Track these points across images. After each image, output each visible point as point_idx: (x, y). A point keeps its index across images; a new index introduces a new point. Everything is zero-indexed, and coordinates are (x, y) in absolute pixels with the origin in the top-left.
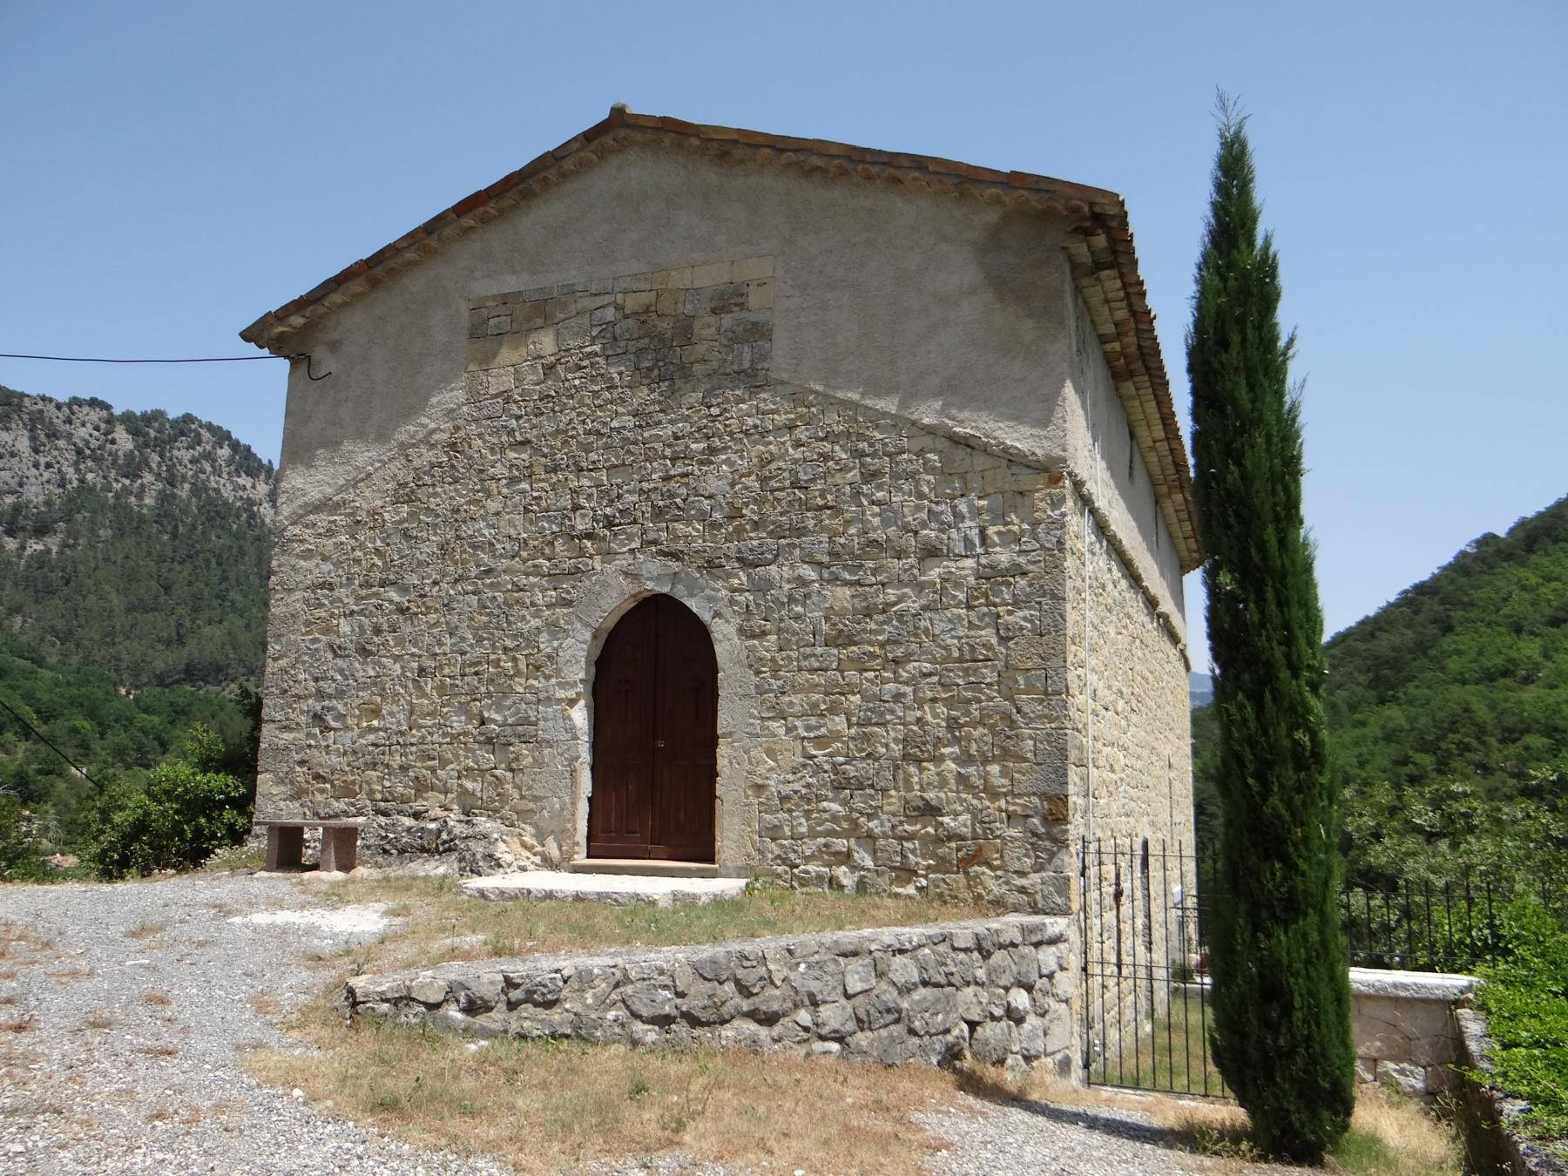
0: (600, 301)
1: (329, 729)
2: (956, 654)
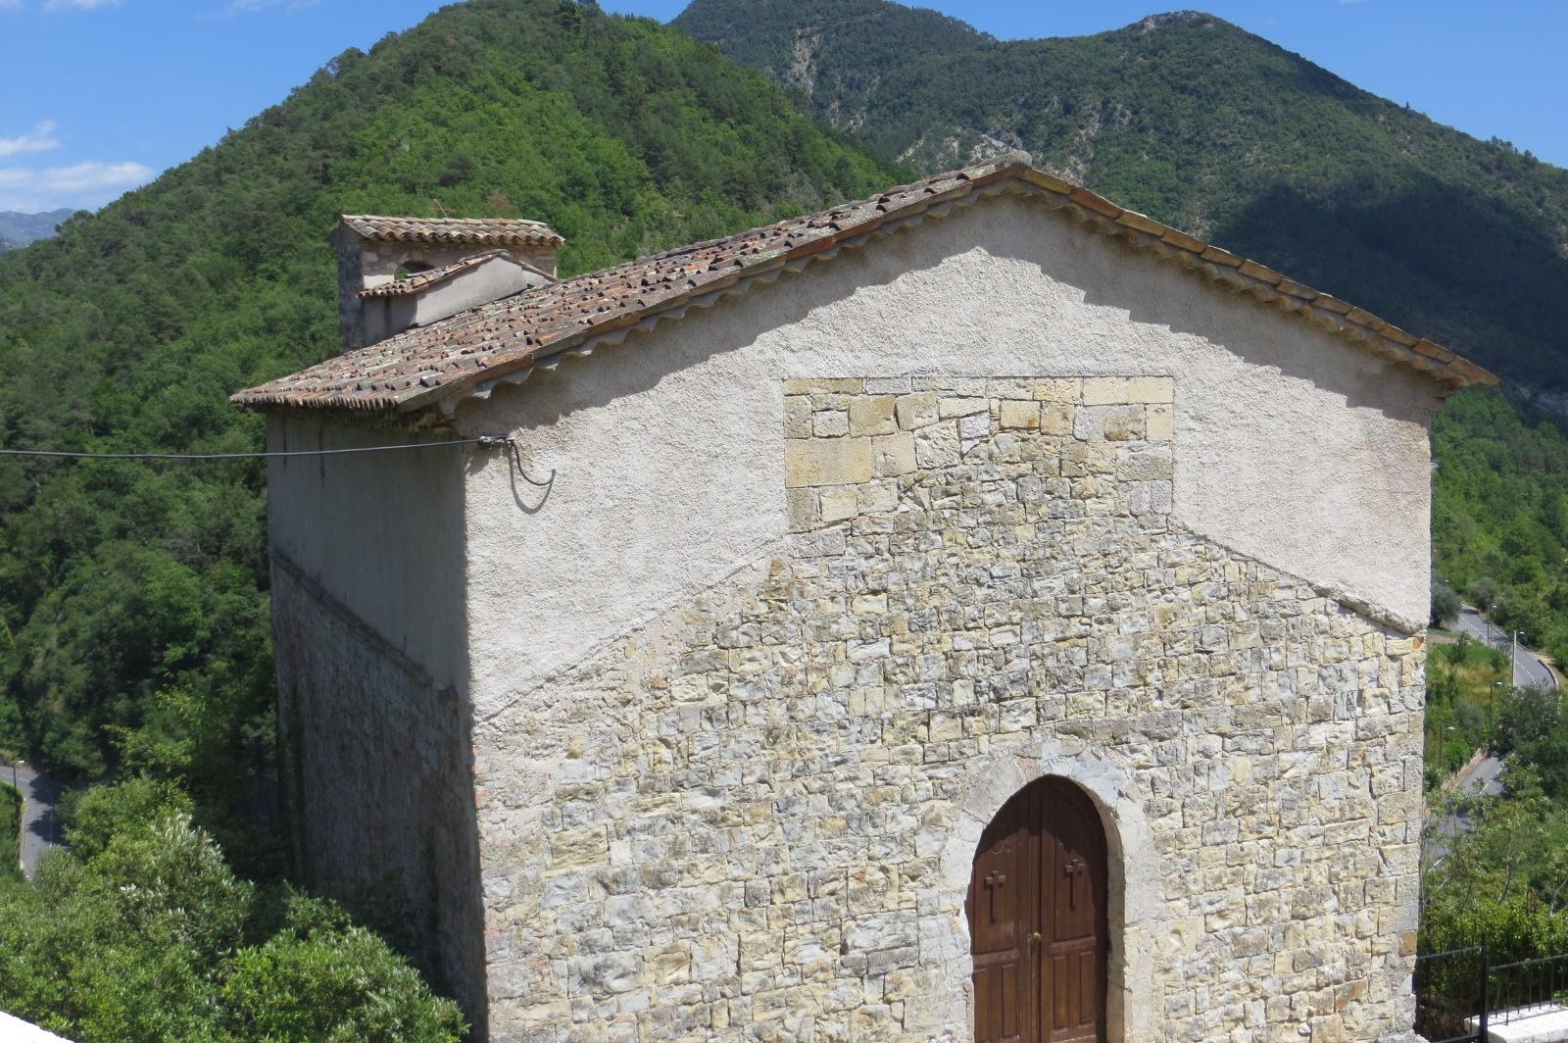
0: (968, 406)
1: (610, 993)
2: (1338, 815)
